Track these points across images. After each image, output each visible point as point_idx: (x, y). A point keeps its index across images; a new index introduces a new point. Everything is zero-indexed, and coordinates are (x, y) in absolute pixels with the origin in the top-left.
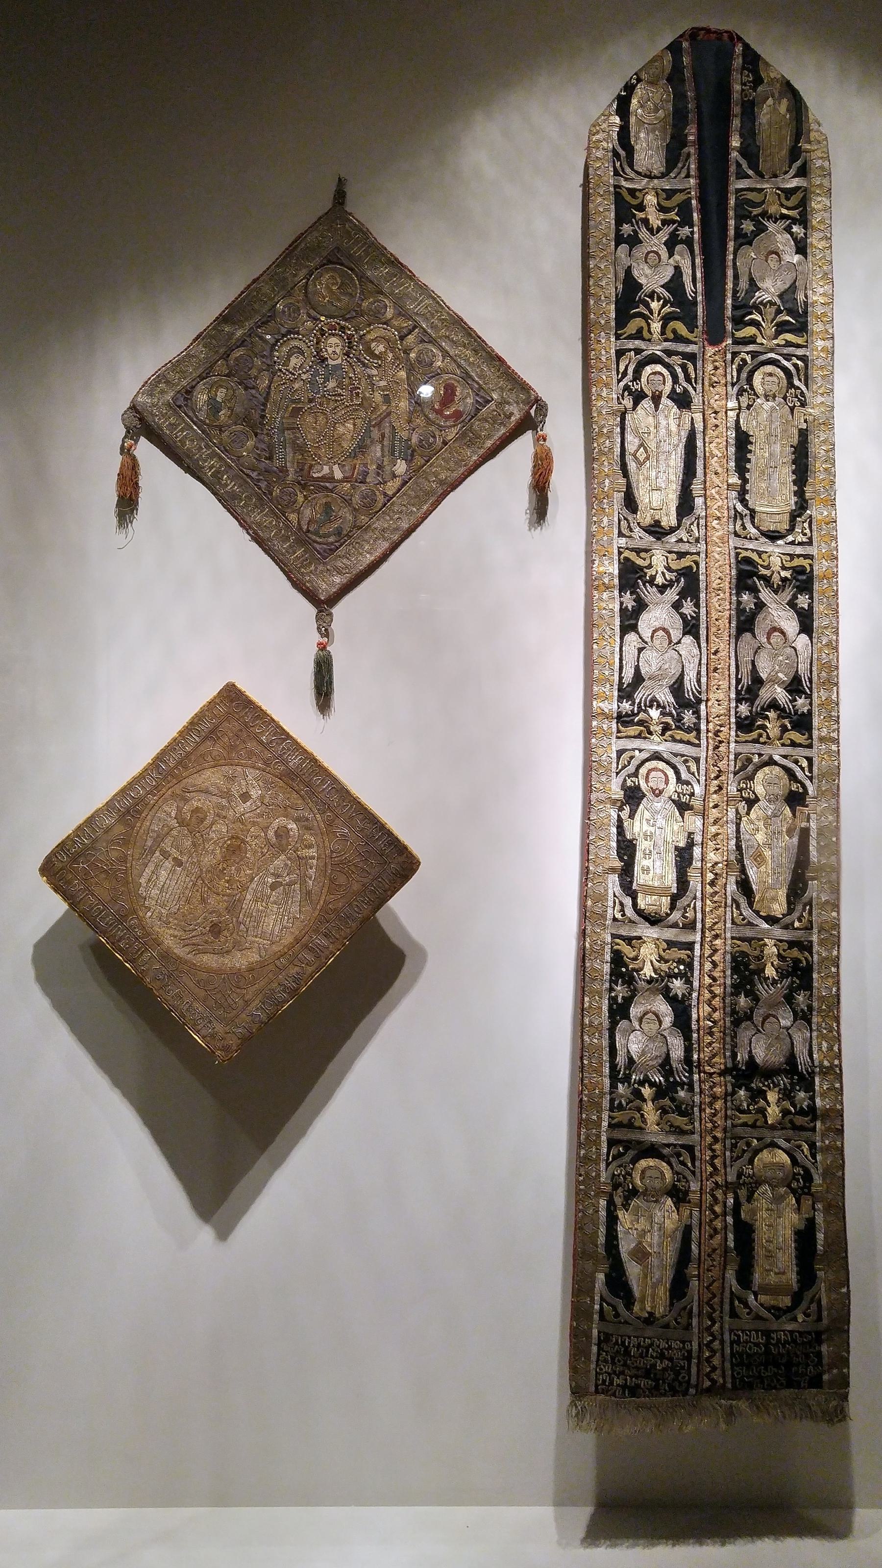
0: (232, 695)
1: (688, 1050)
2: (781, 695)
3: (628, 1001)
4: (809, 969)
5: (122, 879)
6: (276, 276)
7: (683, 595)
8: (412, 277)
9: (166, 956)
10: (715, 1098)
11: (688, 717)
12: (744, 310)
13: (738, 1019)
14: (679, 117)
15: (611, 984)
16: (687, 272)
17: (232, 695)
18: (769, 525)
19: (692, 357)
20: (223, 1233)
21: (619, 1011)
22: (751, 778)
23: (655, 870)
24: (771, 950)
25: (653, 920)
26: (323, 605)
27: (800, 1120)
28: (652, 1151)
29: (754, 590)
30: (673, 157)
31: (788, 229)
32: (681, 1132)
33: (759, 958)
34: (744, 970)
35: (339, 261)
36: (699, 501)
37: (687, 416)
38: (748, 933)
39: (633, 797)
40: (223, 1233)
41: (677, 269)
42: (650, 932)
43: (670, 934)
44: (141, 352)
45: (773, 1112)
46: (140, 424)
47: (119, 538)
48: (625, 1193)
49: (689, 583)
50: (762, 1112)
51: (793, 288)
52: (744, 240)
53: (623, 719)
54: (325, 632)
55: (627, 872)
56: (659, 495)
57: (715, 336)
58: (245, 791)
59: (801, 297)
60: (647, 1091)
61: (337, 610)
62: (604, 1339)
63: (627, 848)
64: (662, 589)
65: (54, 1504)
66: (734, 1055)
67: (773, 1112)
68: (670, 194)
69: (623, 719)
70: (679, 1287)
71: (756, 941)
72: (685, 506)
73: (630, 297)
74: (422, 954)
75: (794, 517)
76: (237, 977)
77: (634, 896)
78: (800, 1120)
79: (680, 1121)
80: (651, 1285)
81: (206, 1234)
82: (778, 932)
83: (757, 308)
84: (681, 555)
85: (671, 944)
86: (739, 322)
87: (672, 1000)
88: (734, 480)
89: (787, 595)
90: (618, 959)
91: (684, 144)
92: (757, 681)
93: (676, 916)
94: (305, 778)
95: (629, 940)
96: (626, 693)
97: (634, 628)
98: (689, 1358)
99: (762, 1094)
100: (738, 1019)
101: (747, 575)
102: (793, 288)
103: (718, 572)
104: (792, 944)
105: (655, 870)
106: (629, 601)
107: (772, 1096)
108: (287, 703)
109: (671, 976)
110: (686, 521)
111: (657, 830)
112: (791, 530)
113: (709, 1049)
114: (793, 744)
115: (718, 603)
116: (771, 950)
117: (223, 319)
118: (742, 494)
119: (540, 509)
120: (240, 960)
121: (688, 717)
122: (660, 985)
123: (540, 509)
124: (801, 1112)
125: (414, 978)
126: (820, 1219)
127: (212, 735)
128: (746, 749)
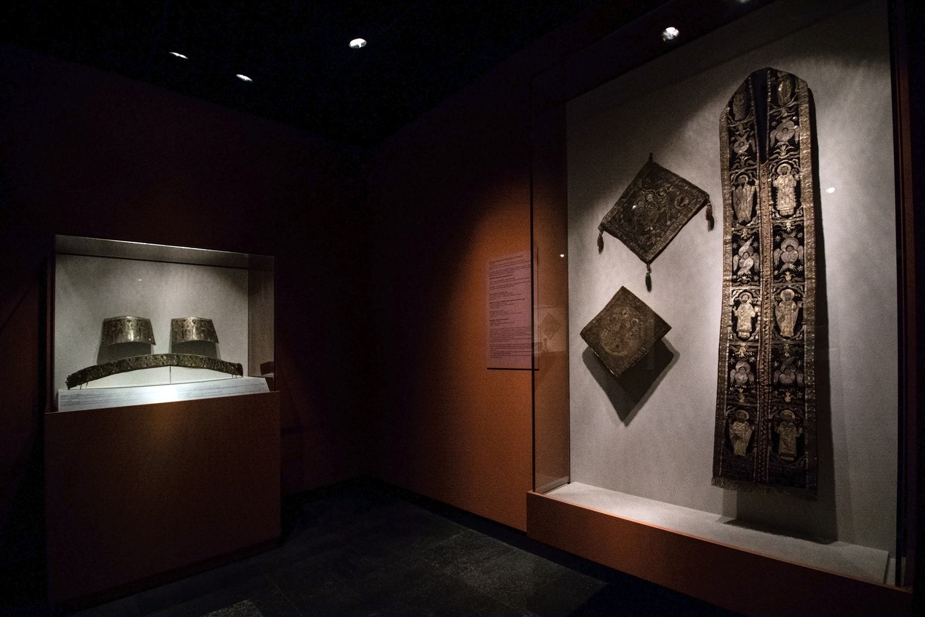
0: (623, 289)
1: (755, 379)
2: (792, 266)
3: (735, 364)
4: (803, 353)
5: (597, 336)
6: (635, 183)
7: (753, 241)
8: (670, 172)
9: (606, 353)
10: (765, 393)
11: (756, 278)
12: (772, 150)
13: (774, 369)
14: (748, 100)
15: (729, 358)
16: (753, 145)
17: (623, 289)
18: (785, 214)
19: (755, 170)
20: (627, 425)
21: (732, 367)
22: (779, 294)
23: (745, 325)
24: (787, 347)
25: (744, 340)
26: (648, 263)
27: (798, 402)
28: (742, 408)
29: (780, 235)
30: (747, 112)
31: (791, 120)
32: (753, 403)
33: (783, 350)
34: (777, 354)
35: (654, 175)
36: (758, 212)
37: (753, 188)
38: (778, 342)
39: (737, 303)
40: (627, 425)
41: (750, 145)
42: (744, 344)
43: (749, 344)
44: (603, 212)
45: (788, 399)
46: (603, 228)
47: (599, 256)
48: (733, 418)
49: (756, 237)
50: (783, 398)
51: (794, 137)
52: (773, 128)
53: (734, 281)
54: (649, 270)
55: (734, 326)
56: (745, 212)
57: (762, 161)
58: (626, 312)
59: (797, 139)
60: (741, 390)
61: (652, 266)
62: (724, 461)
63: (735, 319)
64: (746, 241)
65: (765, 531)
66: (772, 380)
67: (788, 399)
68: (746, 123)
69: (734, 281)
70: (749, 449)
71: (782, 344)
72: (754, 213)
73: (734, 156)
74: (678, 354)
75: (795, 209)
76: (621, 358)
77: (737, 333)
78: (798, 402)
79: (752, 399)
80: (739, 448)
81: (622, 425)
82: (789, 341)
83: (778, 148)
84: (752, 229)
85: (750, 347)
86: (771, 154)
87: (750, 364)
88: (772, 202)
89: (793, 235)
90: (731, 352)
91: (750, 106)
92: (781, 263)
93: (752, 338)
94: (640, 307)
95: (735, 346)
96: (735, 273)
97: (737, 254)
98: (753, 470)
99: (784, 393)
100: (774, 369)
101: (778, 231)
102: (794, 137)
103: (766, 231)
104: (795, 346)
105: (745, 325)
106: (735, 246)
107: (788, 394)
108: (639, 291)
109: (750, 356)
110: (754, 219)
111: (747, 312)
112: (795, 213)
113: (764, 379)
114: (796, 281)
115: (767, 241)
116: (787, 347)
117: (622, 198)
118: (775, 206)
119: (711, 226)
120: (624, 353)
121: (756, 278)
122: (746, 359)
123: (711, 226)
124: (799, 399)
125: (676, 361)
126: (807, 435)
127: (618, 299)
128: (777, 285)
